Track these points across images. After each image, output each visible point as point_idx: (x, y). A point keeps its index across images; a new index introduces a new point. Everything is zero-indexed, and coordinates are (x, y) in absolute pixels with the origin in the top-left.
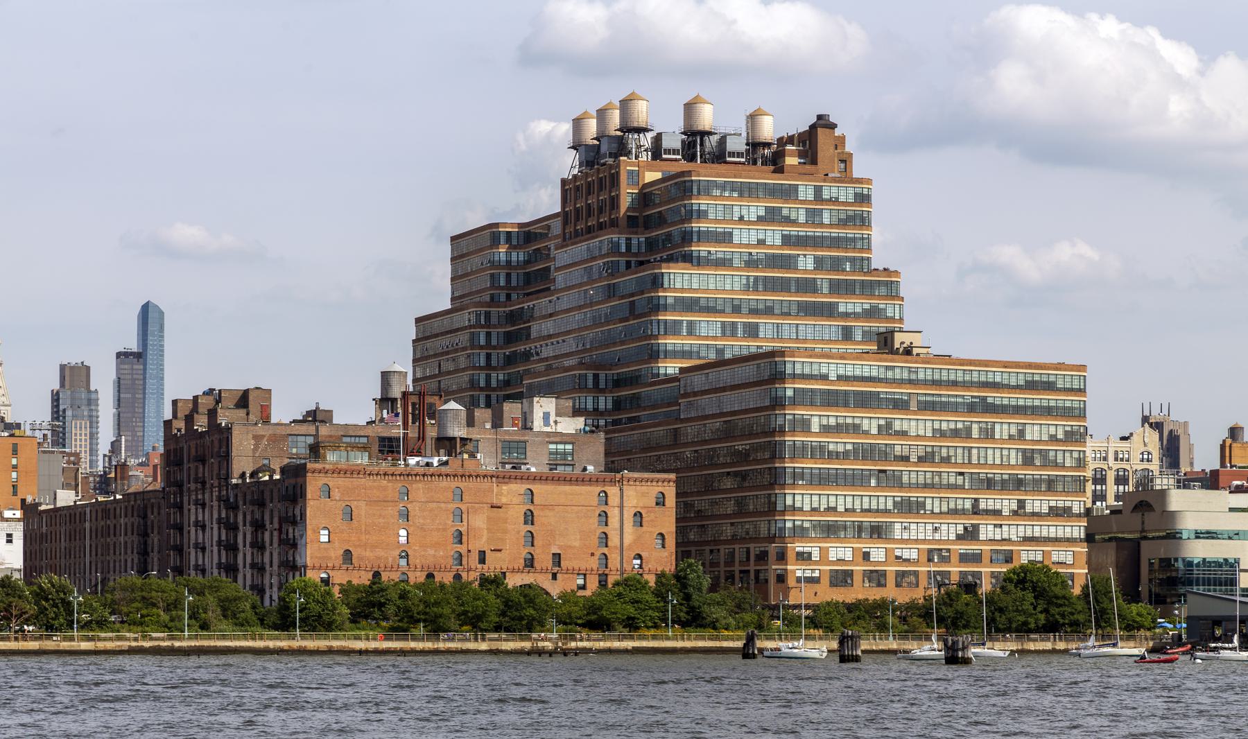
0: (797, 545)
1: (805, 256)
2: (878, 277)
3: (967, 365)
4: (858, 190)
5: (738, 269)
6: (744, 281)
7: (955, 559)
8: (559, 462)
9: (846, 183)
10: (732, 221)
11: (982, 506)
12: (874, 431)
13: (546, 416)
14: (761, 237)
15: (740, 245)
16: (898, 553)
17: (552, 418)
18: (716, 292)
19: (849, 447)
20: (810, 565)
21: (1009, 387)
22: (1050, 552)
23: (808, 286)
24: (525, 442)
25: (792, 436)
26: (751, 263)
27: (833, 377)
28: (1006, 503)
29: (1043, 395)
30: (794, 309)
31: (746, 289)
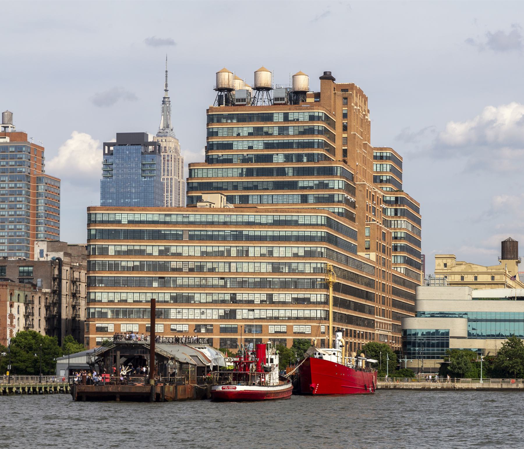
0: (96, 322)
1: (277, 154)
2: (323, 164)
3: (227, 212)
4: (311, 114)
5: (236, 164)
6: (240, 171)
7: (216, 330)
8: (24, 277)
9: (303, 110)
10: (232, 136)
11: (239, 297)
12: (156, 253)
13: (42, 252)
14: (250, 145)
15: (238, 150)
16: (173, 327)
17: (45, 253)
18: (223, 178)
19: (138, 264)
20: (106, 334)
21: (260, 224)
22: (292, 326)
23: (281, 172)
24: (5, 266)
25: (94, 258)
26: (245, 160)
27: (125, 221)
28: (258, 296)
29: (287, 228)
30: (271, 186)
31: (241, 175)
